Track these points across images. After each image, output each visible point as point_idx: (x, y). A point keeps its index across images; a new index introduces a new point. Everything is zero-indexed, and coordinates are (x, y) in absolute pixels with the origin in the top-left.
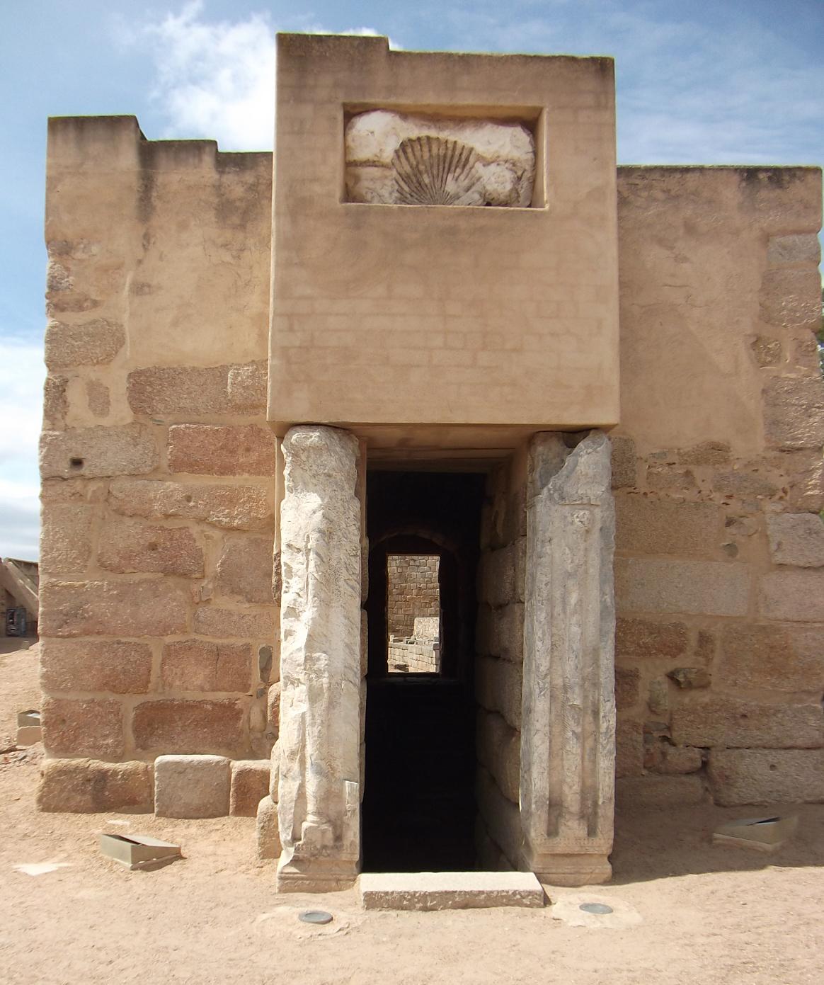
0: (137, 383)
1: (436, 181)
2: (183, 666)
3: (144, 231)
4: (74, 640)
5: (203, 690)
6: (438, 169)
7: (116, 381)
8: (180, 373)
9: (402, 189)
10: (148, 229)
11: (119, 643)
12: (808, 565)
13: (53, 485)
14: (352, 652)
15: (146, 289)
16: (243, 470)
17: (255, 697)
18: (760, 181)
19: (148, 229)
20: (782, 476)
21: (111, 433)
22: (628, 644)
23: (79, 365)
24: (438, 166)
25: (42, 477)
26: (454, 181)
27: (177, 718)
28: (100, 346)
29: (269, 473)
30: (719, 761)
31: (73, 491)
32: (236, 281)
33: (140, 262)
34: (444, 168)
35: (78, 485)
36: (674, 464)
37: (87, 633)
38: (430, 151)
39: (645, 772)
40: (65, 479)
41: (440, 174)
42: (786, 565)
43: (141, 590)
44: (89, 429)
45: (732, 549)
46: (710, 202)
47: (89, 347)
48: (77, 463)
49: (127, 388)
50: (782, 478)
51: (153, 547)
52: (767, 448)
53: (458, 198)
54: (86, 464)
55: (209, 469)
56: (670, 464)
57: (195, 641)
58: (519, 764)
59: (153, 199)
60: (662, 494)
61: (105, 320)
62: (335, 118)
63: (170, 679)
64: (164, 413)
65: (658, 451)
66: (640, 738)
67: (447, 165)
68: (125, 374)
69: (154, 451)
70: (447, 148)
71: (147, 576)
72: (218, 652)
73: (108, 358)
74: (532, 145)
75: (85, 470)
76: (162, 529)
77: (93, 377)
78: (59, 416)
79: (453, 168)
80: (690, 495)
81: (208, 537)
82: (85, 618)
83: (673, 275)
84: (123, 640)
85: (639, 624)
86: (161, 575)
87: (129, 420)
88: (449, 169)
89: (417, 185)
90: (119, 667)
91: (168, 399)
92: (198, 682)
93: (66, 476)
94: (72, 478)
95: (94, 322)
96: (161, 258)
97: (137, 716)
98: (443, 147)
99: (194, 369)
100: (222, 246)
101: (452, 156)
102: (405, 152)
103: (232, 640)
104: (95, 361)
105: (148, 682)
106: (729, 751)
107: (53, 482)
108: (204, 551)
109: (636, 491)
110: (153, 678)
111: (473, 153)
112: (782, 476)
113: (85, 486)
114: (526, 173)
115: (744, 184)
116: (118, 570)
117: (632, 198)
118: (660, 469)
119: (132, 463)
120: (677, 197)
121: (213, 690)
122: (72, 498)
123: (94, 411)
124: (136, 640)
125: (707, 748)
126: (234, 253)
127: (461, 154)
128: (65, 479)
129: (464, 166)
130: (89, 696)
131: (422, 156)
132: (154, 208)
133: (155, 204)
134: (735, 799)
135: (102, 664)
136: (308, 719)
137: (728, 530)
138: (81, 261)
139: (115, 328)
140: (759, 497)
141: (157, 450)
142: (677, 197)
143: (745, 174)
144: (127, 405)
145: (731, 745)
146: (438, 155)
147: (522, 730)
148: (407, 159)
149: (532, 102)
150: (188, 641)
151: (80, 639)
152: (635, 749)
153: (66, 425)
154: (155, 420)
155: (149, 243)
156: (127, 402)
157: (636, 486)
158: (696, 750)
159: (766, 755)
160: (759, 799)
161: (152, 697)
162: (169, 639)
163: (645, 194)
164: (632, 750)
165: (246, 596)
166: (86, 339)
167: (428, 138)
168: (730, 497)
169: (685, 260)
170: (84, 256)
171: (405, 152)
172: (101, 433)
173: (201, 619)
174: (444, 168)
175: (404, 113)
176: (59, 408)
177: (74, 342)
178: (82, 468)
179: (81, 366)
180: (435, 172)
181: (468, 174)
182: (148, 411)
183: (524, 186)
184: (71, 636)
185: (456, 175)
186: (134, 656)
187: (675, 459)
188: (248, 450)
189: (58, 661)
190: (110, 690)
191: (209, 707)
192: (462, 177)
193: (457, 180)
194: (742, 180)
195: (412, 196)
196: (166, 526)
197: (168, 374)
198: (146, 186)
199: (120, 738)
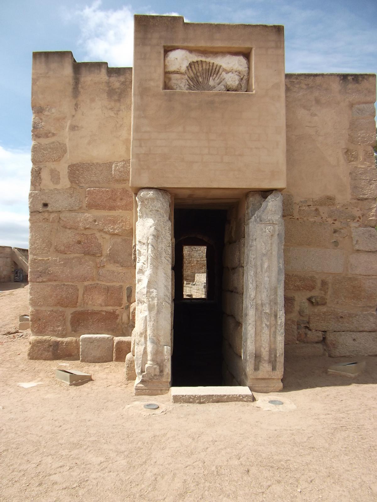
0: (72, 169)
1: (205, 80)
3: (74, 103)
4: (44, 284)
5: (101, 306)
6: (206, 75)
7: (63, 169)
9: (190, 84)
11: (64, 285)
12: (370, 250)
14: (168, 289)
15: (76, 128)
16: (119, 209)
17: (124, 309)
20: (358, 211)
22: (290, 285)
24: (206, 73)
26: (213, 80)
27: (90, 318)
28: (56, 153)
31: (44, 218)
33: (73, 116)
35: (46, 215)
36: (310, 205)
37: (50, 280)
38: (202, 67)
39: (297, 342)
40: (40, 212)
42: (360, 250)
43: (59, 351)
45: (336, 243)
46: (326, 89)
47: (51, 154)
48: (45, 205)
50: (359, 212)
51: (79, 242)
54: (49, 206)
55: (104, 208)
56: (309, 206)
57: (98, 284)
58: (242, 339)
59: (79, 88)
60: (305, 219)
61: (58, 142)
62: (160, 52)
63: (87, 301)
64: (84, 183)
66: (296, 327)
67: (210, 73)
68: (67, 166)
70: (210, 66)
71: (77, 255)
72: (108, 289)
73: (59, 159)
75: (49, 208)
76: (83, 234)
77: (53, 167)
78: (37, 184)
79: (212, 74)
80: (318, 219)
81: (103, 238)
84: (66, 284)
86: (83, 255)
87: (69, 186)
88: (211, 75)
89: (196, 82)
90: (64, 296)
92: (99, 302)
93: (41, 211)
94: (44, 212)
95: (53, 143)
96: (83, 115)
98: (208, 65)
99: (97, 163)
101: (212, 69)
102: (191, 67)
104: (54, 160)
105: (77, 302)
107: (35, 214)
108: (102, 244)
110: (79, 300)
112: (358, 211)
113: (49, 215)
114: (245, 77)
115: (341, 82)
116: (64, 252)
117: (292, 87)
118: (304, 208)
120: (312, 87)
125: (325, 332)
126: (115, 112)
127: (216, 68)
128: (40, 212)
129: (217, 74)
131: (199, 69)
132: (79, 92)
133: (80, 90)
134: (337, 354)
135: (57, 294)
136: (148, 319)
137: (335, 235)
138: (47, 116)
140: (348, 220)
142: (312, 87)
143: (342, 77)
147: (243, 324)
148: (192, 70)
149: (247, 45)
150: (94, 284)
152: (293, 332)
153: (41, 188)
154: (81, 186)
155: (77, 108)
159: (351, 335)
160: (348, 354)
161: (79, 309)
162: (86, 283)
163: (297, 86)
166: (49, 150)
167: (201, 61)
168: (335, 220)
169: (315, 115)
170: (49, 114)
171: (191, 67)
173: (100, 274)
175: (191, 50)
176: (38, 181)
177: (44, 152)
179: (47, 162)
180: (204, 76)
182: (77, 182)
183: (244, 82)
184: (43, 282)
185: (214, 77)
186: (71, 291)
187: (311, 203)
188: (121, 199)
190: (60, 306)
191: (104, 313)
192: (216, 79)
193: (214, 80)
195: (194, 87)
198: (76, 83)
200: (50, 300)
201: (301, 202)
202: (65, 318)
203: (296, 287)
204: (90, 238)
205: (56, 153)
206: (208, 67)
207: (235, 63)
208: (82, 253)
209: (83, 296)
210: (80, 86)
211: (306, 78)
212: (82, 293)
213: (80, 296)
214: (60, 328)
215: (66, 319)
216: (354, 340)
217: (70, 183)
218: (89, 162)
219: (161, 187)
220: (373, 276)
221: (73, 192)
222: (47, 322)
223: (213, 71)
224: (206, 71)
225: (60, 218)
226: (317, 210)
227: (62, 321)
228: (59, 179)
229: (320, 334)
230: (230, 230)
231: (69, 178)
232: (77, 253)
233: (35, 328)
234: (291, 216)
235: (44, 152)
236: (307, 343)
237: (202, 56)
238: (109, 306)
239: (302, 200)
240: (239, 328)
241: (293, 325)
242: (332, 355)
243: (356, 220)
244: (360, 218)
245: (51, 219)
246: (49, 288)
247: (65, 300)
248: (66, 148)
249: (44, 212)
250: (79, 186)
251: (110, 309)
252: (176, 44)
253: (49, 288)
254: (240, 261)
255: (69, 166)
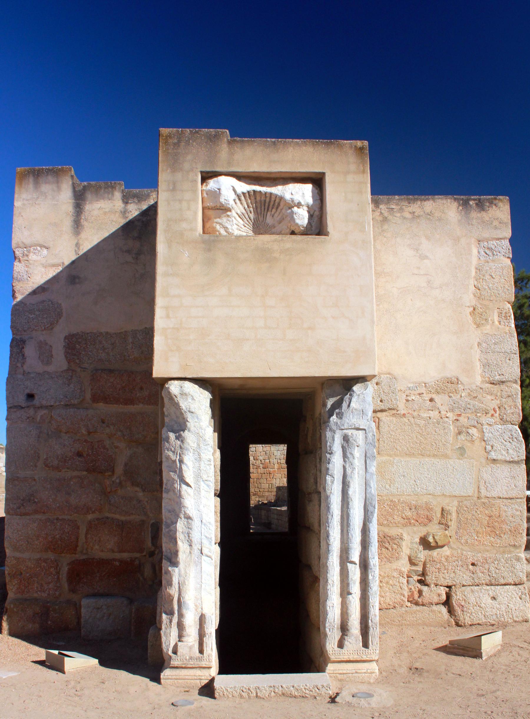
0: (71, 342)
1: (260, 217)
2: (100, 535)
3: (76, 241)
4: (28, 517)
5: (113, 551)
6: (261, 210)
7: (57, 343)
8: (98, 336)
10: (78, 240)
11: (57, 519)
12: (512, 460)
13: (15, 412)
15: (77, 280)
16: (139, 402)
17: (147, 556)
18: (471, 206)
19: (78, 240)
20: (492, 400)
21: (53, 376)
22: (395, 517)
23: (32, 331)
24: (261, 208)
25: (7, 407)
26: (271, 217)
28: (46, 318)
29: (156, 403)
30: (457, 598)
31: (28, 415)
32: (135, 274)
34: (265, 209)
35: (31, 412)
36: (423, 393)
37: (36, 512)
38: (255, 199)
39: (409, 604)
40: (23, 408)
41: (263, 213)
42: (497, 460)
43: (72, 483)
44: (39, 374)
45: (462, 451)
46: (440, 220)
47: (40, 319)
48: (31, 396)
49: (64, 346)
50: (493, 402)
51: (79, 454)
52: (483, 382)
53: (275, 227)
54: (36, 397)
55: (117, 401)
56: (420, 394)
57: (107, 518)
58: (319, 602)
59: (82, 221)
61: (50, 300)
63: (91, 544)
64: (87, 363)
65: (412, 385)
66: (405, 581)
67: (266, 207)
68: (62, 336)
69: (81, 389)
70: (266, 197)
71: (76, 473)
72: (122, 526)
73: (51, 327)
74: (319, 195)
75: (36, 402)
76: (86, 441)
77: (42, 338)
78: (19, 365)
79: (270, 209)
80: (434, 414)
81: (117, 447)
82: (35, 502)
83: (419, 268)
84: (60, 517)
85: (402, 503)
86: (85, 473)
87: (65, 367)
88: (268, 210)
90: (58, 536)
91: (91, 354)
92: (109, 547)
93: (23, 405)
94: (28, 407)
95: (43, 301)
97: (69, 569)
99: (107, 333)
100: (126, 252)
101: (270, 202)
103: (132, 517)
104: (43, 328)
105: (77, 546)
106: (464, 588)
107: (15, 410)
108: (113, 456)
109: (398, 412)
110: (80, 544)
111: (282, 200)
112: (492, 400)
113: (36, 412)
114: (316, 213)
115: (461, 208)
116: (57, 469)
117: (390, 217)
119: (67, 397)
120: (419, 217)
121: (120, 552)
122: (28, 420)
123: (42, 361)
124: (69, 517)
125: (449, 587)
126: (134, 256)
127: (275, 201)
128: (23, 408)
129: (277, 208)
130: (37, 556)
132: (82, 226)
133: (83, 224)
134: (468, 621)
135: (47, 534)
137: (459, 437)
139: (56, 306)
140: (478, 415)
141: (83, 389)
142: (419, 217)
143: (461, 202)
144: (63, 356)
145: (466, 584)
146: (261, 201)
147: (321, 578)
148: (241, 203)
149: (317, 169)
150: (103, 518)
151: (32, 517)
152: (401, 588)
153: (24, 371)
154: (82, 368)
156: (63, 355)
157: (398, 409)
158: (442, 588)
159: (488, 590)
160: (484, 621)
161: (79, 556)
162: (90, 517)
163: (399, 215)
164: (400, 589)
165: (142, 488)
166: (37, 313)
167: (254, 191)
168: (459, 415)
169: (426, 257)
172: (47, 376)
174: (265, 209)
175: (239, 177)
176: (20, 360)
177: (29, 315)
178: (34, 400)
179: (34, 331)
181: (280, 213)
182: (77, 361)
183: (315, 221)
184: (26, 514)
185: (273, 213)
187: (423, 390)
188: (141, 388)
189: (17, 531)
190: (52, 551)
191: (117, 564)
192: (276, 215)
193: (273, 216)
194: (459, 205)
196: (89, 440)
197: (91, 336)
198: (78, 212)
199: (58, 585)
200: (36, 542)
201: (410, 389)
202: (58, 570)
203: (404, 519)
204: (96, 446)
205: (46, 318)
206: (264, 199)
207: (303, 193)
208: (84, 471)
209: (86, 538)
210: (83, 217)
211: (409, 203)
212: (84, 531)
213: (82, 538)
214: (51, 586)
215: (61, 573)
216: (494, 598)
217: (67, 363)
218: (95, 331)
219: (198, 378)
220: (517, 498)
221: (72, 376)
222: (31, 577)
223: (272, 204)
224: (261, 204)
225: (51, 416)
226: (431, 400)
227: (54, 575)
228: (52, 356)
229: (443, 591)
230: (306, 432)
231: (66, 356)
232: (77, 470)
233: (14, 586)
234: (393, 409)
235: (29, 315)
236: (423, 605)
237: (255, 185)
238: (124, 552)
239: (409, 386)
240: (317, 584)
241: (401, 578)
242: (460, 622)
243: (490, 414)
244: (495, 411)
245: (39, 418)
246: (36, 525)
247: (59, 542)
248: (62, 310)
249: (28, 407)
250: (80, 367)
251: (125, 556)
252: (218, 169)
253: (36, 525)
254: (316, 483)
255: (66, 338)
